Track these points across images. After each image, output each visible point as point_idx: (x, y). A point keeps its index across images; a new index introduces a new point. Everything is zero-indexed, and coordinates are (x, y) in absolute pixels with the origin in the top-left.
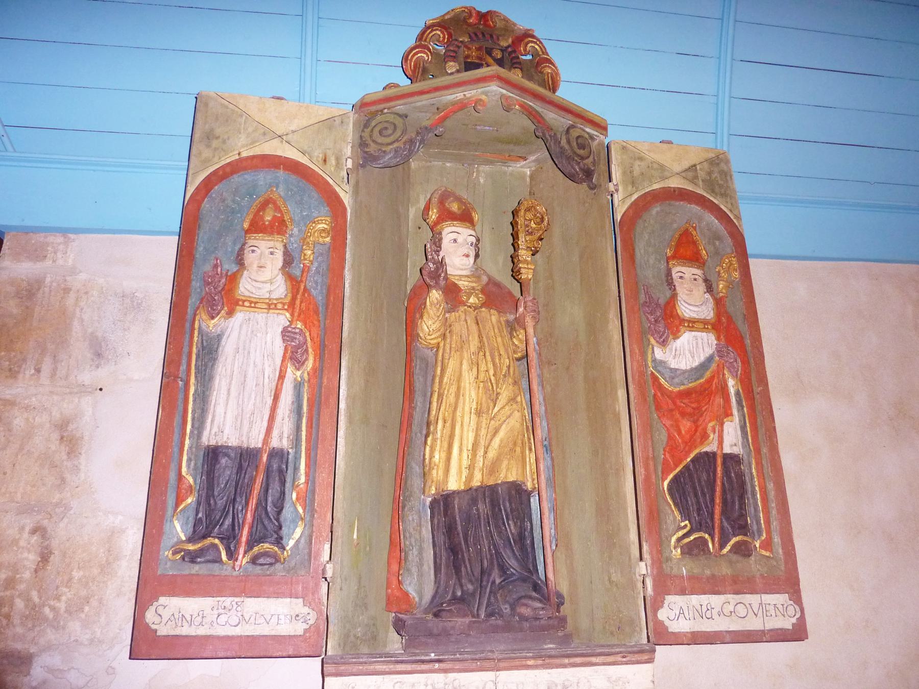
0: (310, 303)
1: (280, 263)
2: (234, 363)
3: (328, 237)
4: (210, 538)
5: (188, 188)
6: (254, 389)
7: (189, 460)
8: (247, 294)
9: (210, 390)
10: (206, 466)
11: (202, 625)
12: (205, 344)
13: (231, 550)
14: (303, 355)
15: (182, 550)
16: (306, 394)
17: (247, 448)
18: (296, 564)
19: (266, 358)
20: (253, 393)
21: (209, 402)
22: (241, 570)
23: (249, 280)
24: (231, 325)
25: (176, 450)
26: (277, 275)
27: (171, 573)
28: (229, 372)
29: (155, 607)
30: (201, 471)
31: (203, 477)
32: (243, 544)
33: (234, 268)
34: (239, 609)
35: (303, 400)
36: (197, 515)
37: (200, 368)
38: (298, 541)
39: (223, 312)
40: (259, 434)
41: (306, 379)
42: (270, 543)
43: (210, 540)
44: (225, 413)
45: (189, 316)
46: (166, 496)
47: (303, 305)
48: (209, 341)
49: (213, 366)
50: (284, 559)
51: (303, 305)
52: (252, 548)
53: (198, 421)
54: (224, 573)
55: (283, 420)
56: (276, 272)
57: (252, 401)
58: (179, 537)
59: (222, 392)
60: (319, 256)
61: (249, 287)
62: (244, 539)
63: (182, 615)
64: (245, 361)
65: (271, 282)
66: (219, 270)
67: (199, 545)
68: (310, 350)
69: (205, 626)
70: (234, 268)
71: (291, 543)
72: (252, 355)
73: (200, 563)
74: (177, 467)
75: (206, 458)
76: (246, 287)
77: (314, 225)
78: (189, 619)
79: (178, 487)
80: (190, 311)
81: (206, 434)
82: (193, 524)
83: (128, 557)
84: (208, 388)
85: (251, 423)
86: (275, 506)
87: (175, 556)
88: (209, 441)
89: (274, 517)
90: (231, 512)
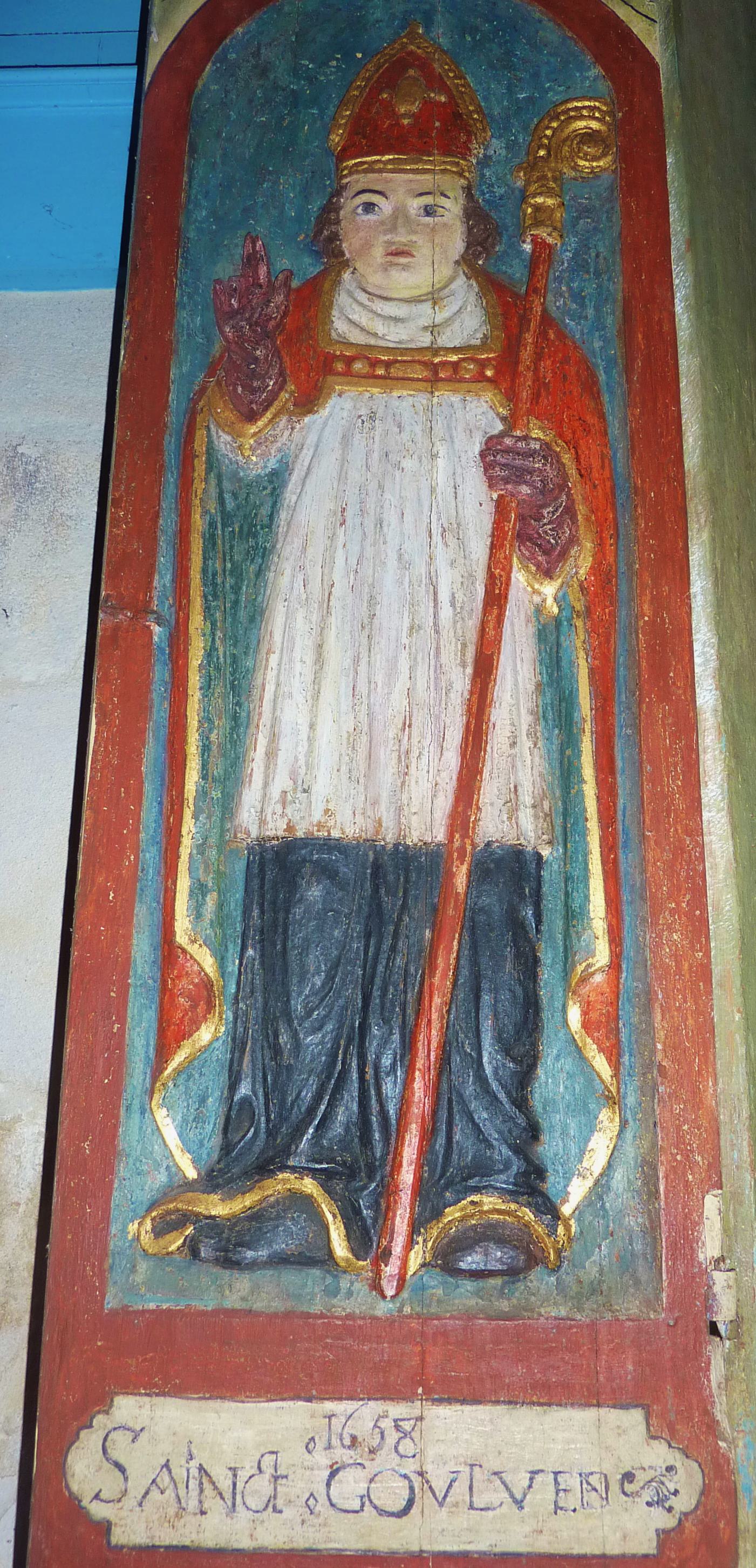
0: (565, 360)
1: (457, 245)
2: (333, 559)
3: (604, 155)
4: (286, 1175)
5: (154, 38)
6: (405, 641)
7: (199, 890)
8: (356, 337)
9: (257, 651)
10: (256, 913)
11: (275, 1510)
12: (230, 504)
13: (363, 1220)
14: (560, 525)
15: (185, 1218)
16: (582, 654)
17: (396, 845)
18: (601, 1272)
19: (437, 538)
20: (405, 654)
21: (256, 693)
22: (405, 1294)
23: (363, 297)
24: (312, 438)
25: (151, 856)
26: (452, 280)
27: (152, 1306)
28: (316, 586)
29: (102, 1434)
30: (239, 928)
31: (250, 952)
32: (405, 1197)
33: (309, 267)
34: (407, 1447)
35: (573, 678)
36: (233, 1086)
37: (219, 580)
38: (601, 1185)
39: (284, 396)
40: (434, 796)
41: (579, 606)
42: (502, 1192)
43: (285, 1181)
44: (312, 726)
45: (174, 418)
46: (122, 1020)
47: (546, 365)
48: (242, 496)
49: (259, 573)
50: (558, 1252)
51: (546, 365)
52: (437, 1214)
53: (224, 755)
54: (343, 1306)
55: (513, 744)
56: (446, 271)
57: (402, 683)
58: (174, 1170)
59: (297, 654)
60: (579, 218)
61: (362, 318)
62: (407, 1176)
63: (201, 1468)
64: (369, 552)
65: (435, 297)
66: (263, 271)
67: (249, 1200)
68: (581, 510)
69: (288, 1513)
70: (309, 267)
71: (578, 1190)
72: (391, 532)
73: (253, 1265)
74: (158, 916)
75: (256, 883)
76: (355, 317)
77: (555, 125)
78: (225, 1484)
79: (164, 989)
80: (175, 400)
81: (250, 797)
82: (220, 1121)
83: (21, 1209)
84: (247, 647)
85: (404, 757)
86: (507, 1051)
87: (162, 1242)
88: (262, 822)
89: (508, 1094)
90: (355, 1076)
